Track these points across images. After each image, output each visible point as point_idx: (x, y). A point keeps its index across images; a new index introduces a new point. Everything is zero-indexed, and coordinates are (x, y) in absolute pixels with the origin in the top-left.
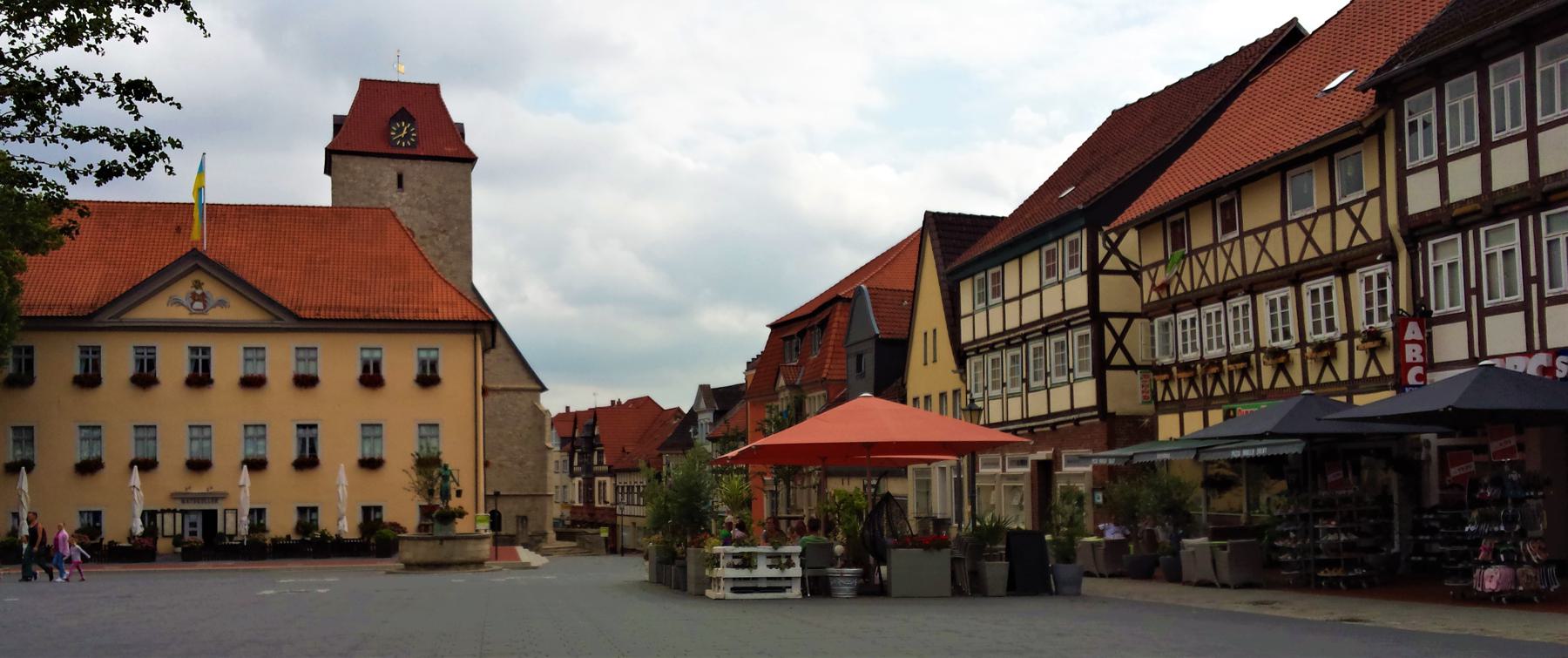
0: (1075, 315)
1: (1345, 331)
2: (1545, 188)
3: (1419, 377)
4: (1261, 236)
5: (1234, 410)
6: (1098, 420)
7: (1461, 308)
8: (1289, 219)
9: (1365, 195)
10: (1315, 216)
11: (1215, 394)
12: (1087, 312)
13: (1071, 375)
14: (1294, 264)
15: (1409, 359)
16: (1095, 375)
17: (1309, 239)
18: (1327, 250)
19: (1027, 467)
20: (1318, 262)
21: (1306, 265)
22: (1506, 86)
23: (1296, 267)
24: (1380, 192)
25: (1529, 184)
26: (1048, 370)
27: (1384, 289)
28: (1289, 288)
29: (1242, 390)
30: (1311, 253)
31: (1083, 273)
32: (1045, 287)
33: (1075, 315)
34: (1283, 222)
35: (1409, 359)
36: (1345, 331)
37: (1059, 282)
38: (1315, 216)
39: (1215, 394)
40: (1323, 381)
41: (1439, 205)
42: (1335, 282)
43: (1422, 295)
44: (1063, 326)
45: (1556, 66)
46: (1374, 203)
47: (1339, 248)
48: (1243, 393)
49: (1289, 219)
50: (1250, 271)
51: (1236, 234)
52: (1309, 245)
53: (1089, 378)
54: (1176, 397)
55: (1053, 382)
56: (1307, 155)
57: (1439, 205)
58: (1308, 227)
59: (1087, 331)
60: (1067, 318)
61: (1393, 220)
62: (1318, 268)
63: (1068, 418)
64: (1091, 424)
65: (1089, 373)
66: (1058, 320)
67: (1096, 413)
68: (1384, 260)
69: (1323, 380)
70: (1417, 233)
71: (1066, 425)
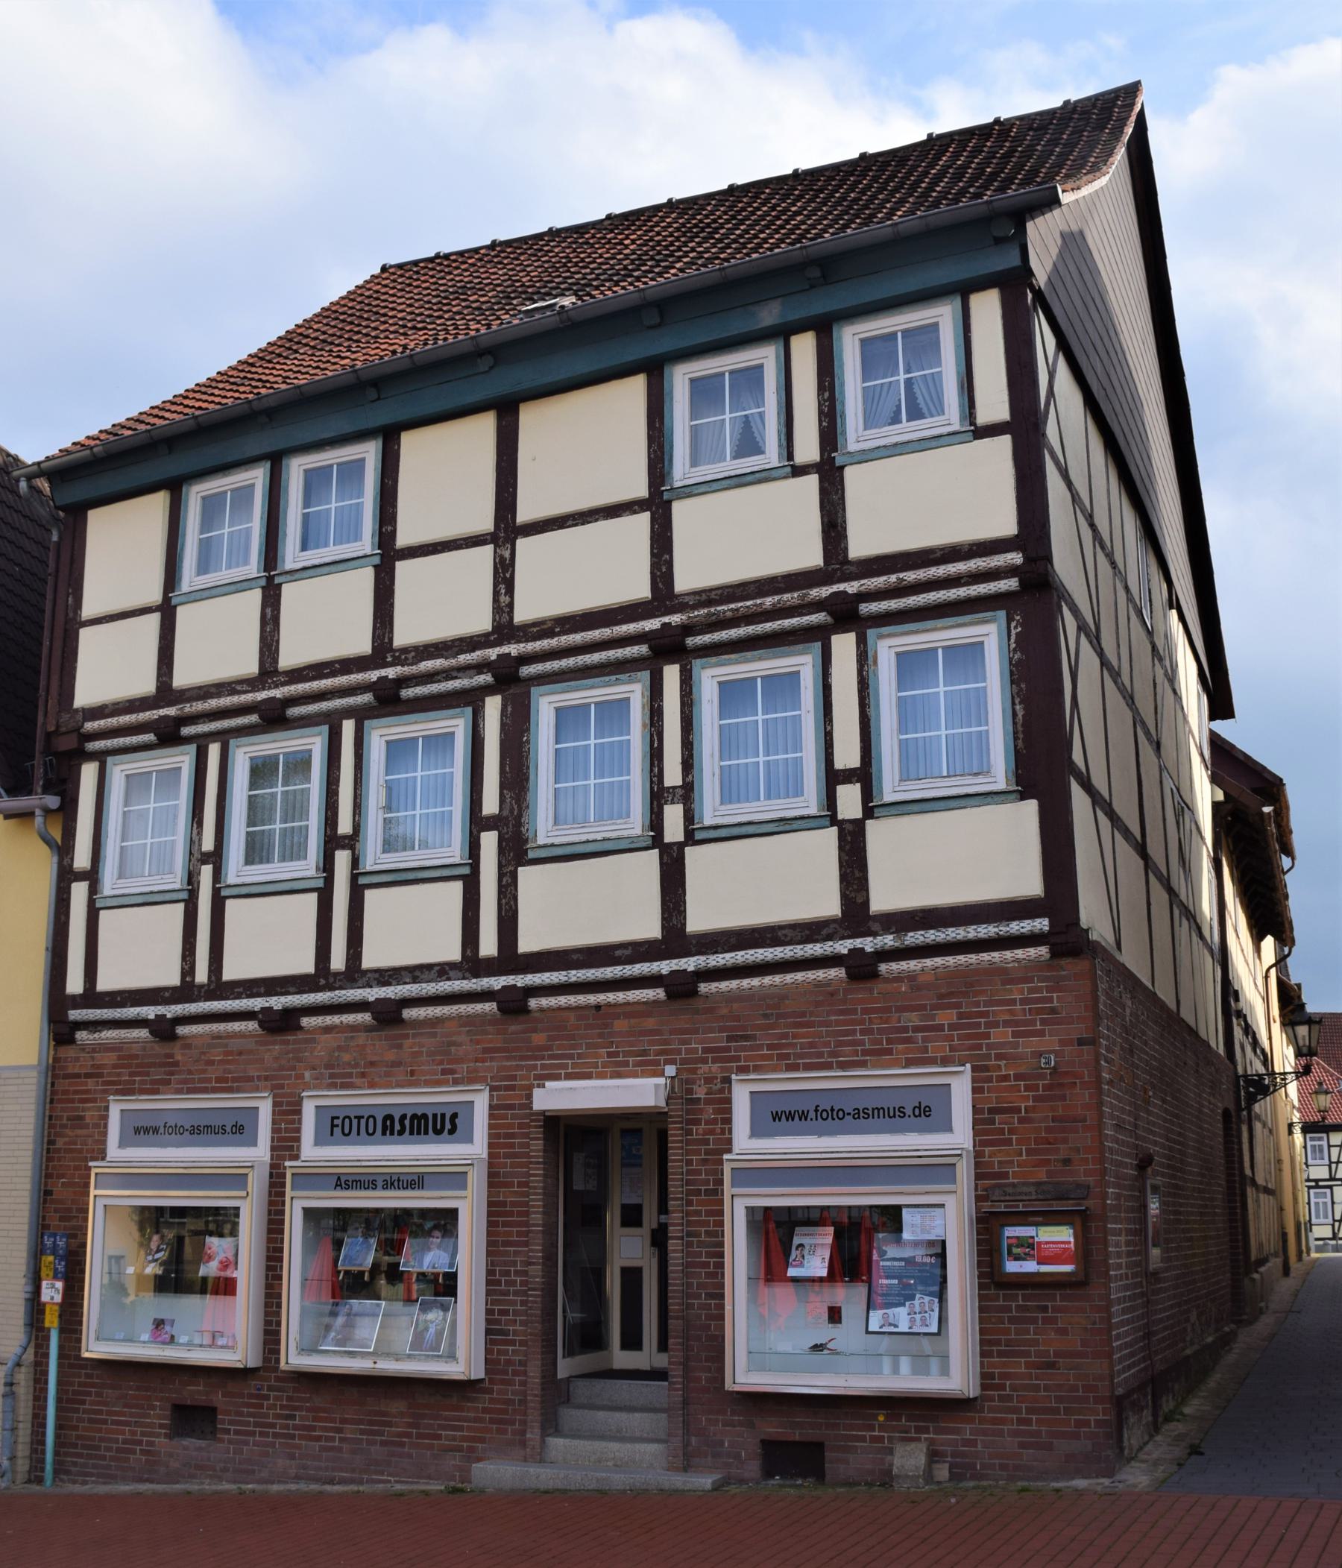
0: (910, 576)
6: (1042, 951)
32: (689, 491)
33: (910, 576)
64: (967, 979)
66: (790, 598)
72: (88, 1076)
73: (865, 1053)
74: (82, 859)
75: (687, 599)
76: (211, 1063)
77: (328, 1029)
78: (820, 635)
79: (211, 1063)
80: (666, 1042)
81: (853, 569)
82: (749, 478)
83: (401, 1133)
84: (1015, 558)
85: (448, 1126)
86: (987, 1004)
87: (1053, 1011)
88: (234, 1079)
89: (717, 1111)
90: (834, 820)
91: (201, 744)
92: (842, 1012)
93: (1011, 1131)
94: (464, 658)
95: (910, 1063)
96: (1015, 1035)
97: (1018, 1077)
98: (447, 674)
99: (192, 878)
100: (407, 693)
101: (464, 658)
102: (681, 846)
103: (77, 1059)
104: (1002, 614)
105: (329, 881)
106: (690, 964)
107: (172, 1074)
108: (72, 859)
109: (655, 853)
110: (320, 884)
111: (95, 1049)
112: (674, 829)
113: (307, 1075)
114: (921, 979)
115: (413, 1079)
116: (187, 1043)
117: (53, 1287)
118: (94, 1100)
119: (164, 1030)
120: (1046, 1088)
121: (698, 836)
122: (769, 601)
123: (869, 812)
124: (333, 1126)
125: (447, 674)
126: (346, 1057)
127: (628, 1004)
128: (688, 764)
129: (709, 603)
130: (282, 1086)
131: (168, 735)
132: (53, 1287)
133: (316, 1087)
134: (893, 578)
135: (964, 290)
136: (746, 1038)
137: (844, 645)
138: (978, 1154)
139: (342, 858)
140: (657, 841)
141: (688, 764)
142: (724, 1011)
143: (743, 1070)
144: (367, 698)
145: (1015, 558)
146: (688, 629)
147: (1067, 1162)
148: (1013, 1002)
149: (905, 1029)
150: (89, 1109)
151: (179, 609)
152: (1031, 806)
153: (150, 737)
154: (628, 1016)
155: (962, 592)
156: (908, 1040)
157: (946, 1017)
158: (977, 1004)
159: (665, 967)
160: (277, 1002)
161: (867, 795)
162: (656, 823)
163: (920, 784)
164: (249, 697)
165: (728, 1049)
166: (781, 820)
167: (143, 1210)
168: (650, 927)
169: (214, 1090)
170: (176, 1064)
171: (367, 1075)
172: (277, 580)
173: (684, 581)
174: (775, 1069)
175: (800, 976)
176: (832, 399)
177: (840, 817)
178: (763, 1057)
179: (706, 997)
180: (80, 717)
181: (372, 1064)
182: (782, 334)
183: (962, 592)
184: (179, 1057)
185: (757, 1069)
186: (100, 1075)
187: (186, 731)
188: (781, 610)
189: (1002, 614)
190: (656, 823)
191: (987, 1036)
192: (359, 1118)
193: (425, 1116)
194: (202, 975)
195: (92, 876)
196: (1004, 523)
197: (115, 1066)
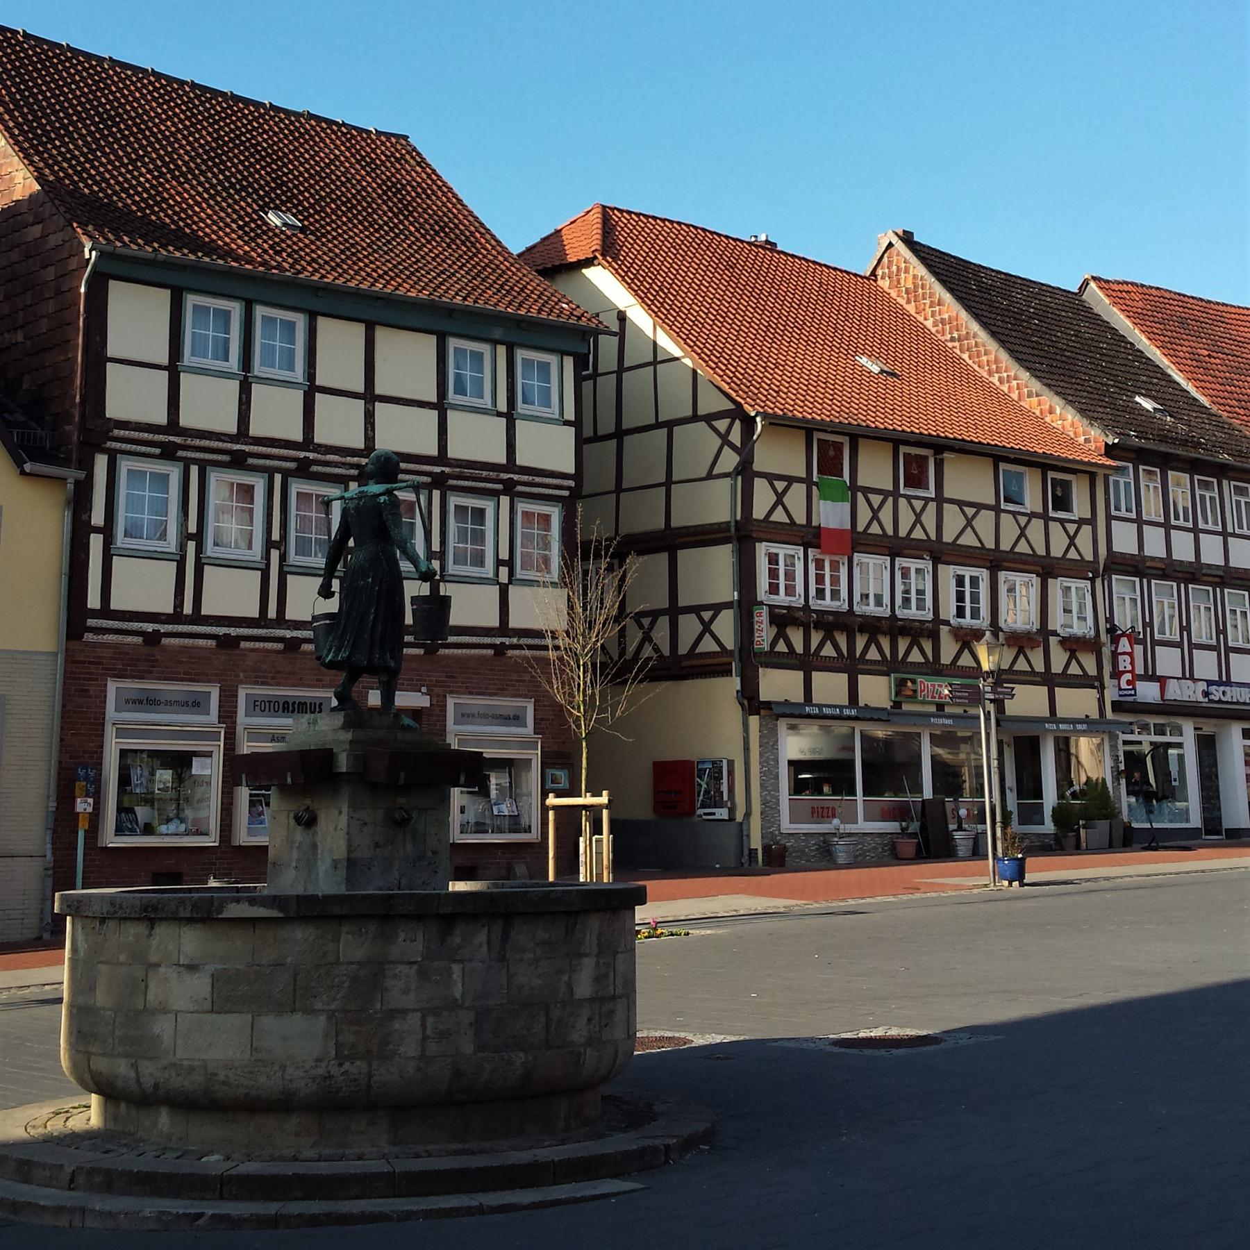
0: (538, 479)
3: (1128, 682)
14: (1003, 551)
15: (1121, 668)
20: (1030, 559)
24: (1092, 521)
33: (538, 479)
35: (1121, 668)
40: (1016, 668)
54: (799, 649)
62: (1026, 563)
63: (487, 640)
66: (493, 475)
69: (1016, 668)
72: (90, 663)
74: (98, 518)
76: (181, 662)
77: (253, 650)
79: (181, 662)
80: (421, 675)
83: (293, 711)
84: (572, 483)
85: (318, 709)
88: (196, 674)
89: (441, 711)
90: (498, 583)
91: (187, 463)
94: (349, 459)
98: (336, 465)
99: (182, 548)
100: (315, 468)
101: (349, 459)
102: (439, 581)
103: (83, 651)
105: (268, 565)
107: (153, 667)
108: (90, 517)
110: (178, 558)
111: (95, 645)
113: (241, 675)
115: (300, 684)
116: (165, 649)
117: (86, 802)
118: (97, 680)
119: (152, 639)
121: (447, 578)
122: (485, 473)
123: (510, 582)
124: (255, 706)
125: (336, 465)
126: (264, 667)
128: (443, 542)
130: (226, 680)
131: (168, 453)
132: (86, 802)
133: (246, 683)
134: (531, 478)
136: (453, 677)
139: (275, 554)
141: (443, 542)
143: (451, 692)
144: (292, 465)
145: (572, 483)
146: (450, 476)
147: (564, 743)
150: (92, 685)
153: (158, 451)
155: (550, 491)
156: (513, 685)
160: (233, 631)
161: (511, 573)
164: (229, 446)
165: (445, 682)
169: (182, 680)
170: (156, 661)
171: (275, 678)
172: (250, 380)
174: (464, 693)
175: (477, 651)
178: (459, 687)
180: (112, 425)
181: (279, 672)
183: (550, 491)
184: (158, 657)
185: (457, 692)
186: (102, 664)
187: (180, 453)
192: (270, 702)
193: (305, 703)
194: (188, 609)
195: (108, 530)
197: (112, 658)
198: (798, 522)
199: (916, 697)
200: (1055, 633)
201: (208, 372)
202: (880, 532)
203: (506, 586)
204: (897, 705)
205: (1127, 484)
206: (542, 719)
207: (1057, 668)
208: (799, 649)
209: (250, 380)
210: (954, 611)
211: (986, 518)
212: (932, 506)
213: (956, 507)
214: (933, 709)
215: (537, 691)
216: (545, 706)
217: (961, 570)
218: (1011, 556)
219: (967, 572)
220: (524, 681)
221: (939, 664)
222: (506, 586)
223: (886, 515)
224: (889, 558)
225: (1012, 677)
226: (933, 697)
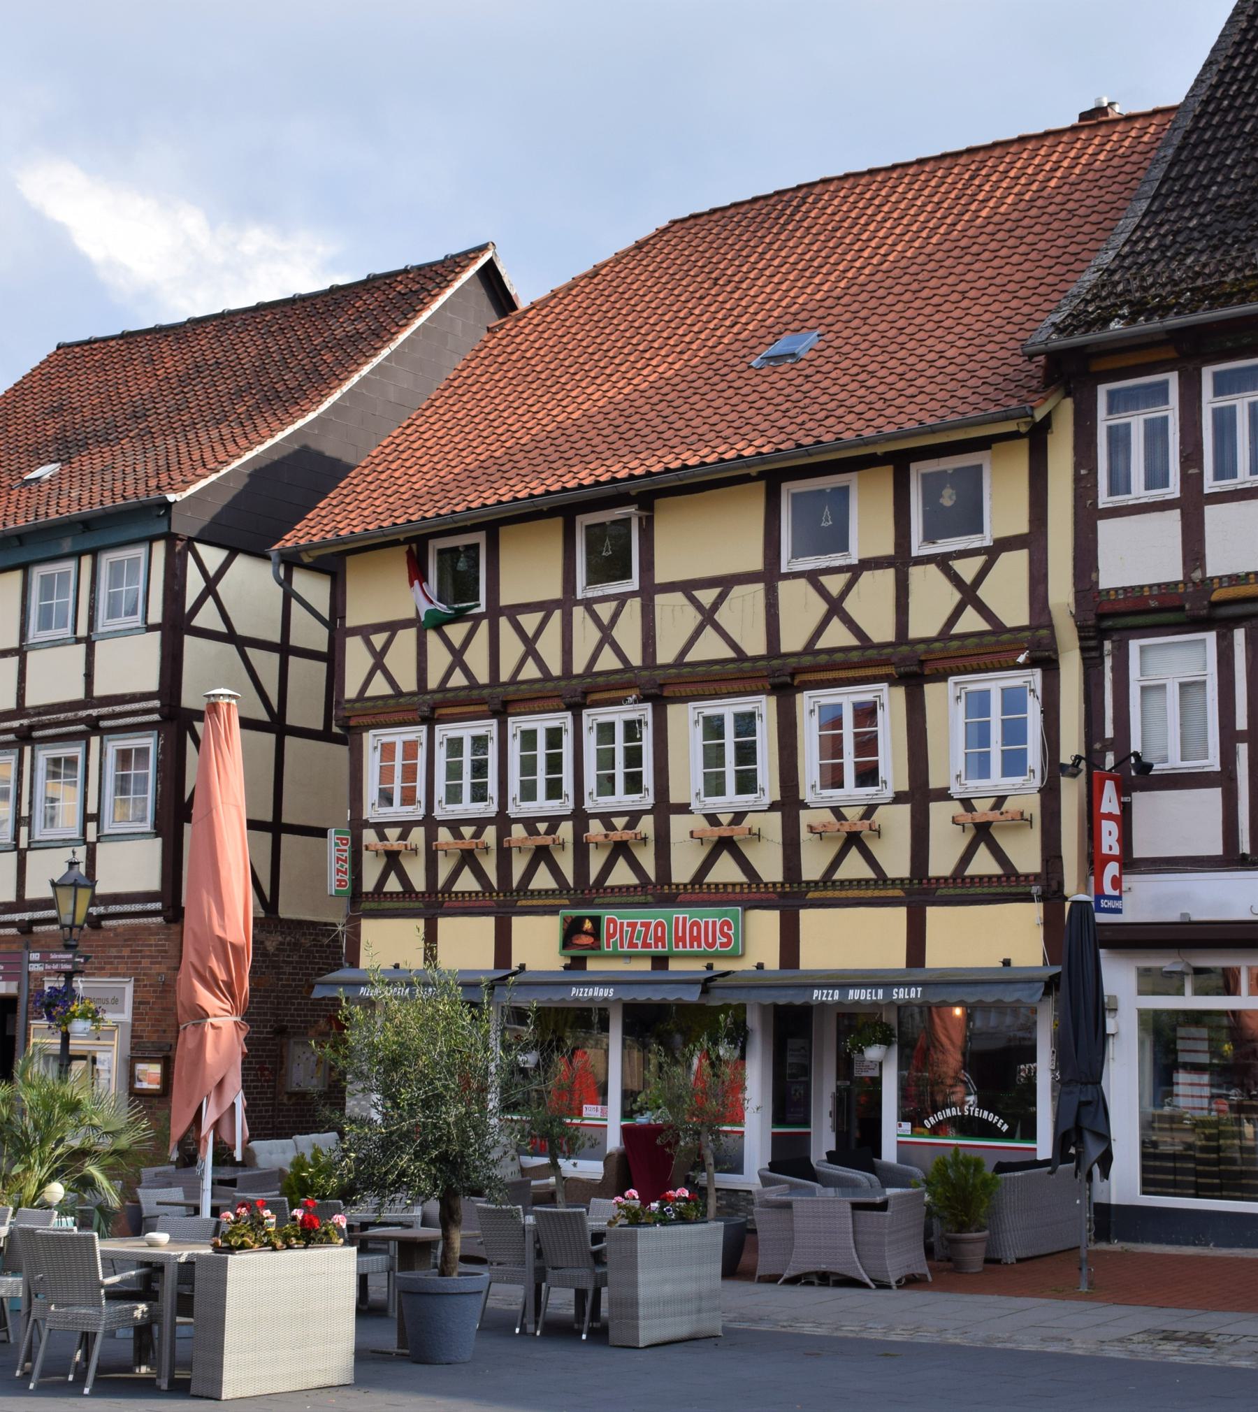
0: (118, 709)
1: (904, 786)
2: (1215, 597)
4: (378, 640)
5: (596, 921)
6: (160, 919)
7: (1213, 763)
8: (784, 569)
9: (988, 542)
10: (856, 571)
11: (386, 889)
12: (156, 703)
13: (24, 831)
16: (158, 830)
17: (379, 664)
18: (408, 683)
19: (123, 1012)
20: (855, 656)
21: (823, 658)
22: (1137, 423)
23: (793, 660)
25: (1181, 586)
26: (25, 812)
27: (612, 746)
28: (763, 697)
29: (612, 881)
30: (531, 671)
31: (150, 628)
32: (35, 647)
33: (118, 709)
34: (567, 602)
36: (904, 786)
37: (78, 641)
38: (856, 571)
39: (386, 889)
41: (1180, 578)
42: (765, 707)
43: (1109, 733)
44: (82, 727)
45: (1241, 403)
46: (1015, 564)
47: (915, 632)
48: (612, 888)
49: (784, 569)
50: (578, 667)
51: (634, 584)
52: (379, 675)
53: (143, 835)
54: (419, 884)
55: (37, 837)
56: (466, 526)
57: (1180, 578)
58: (605, 617)
59: (149, 742)
60: (94, 712)
61: (1061, 592)
64: (134, 929)
65: (147, 826)
66: (70, 715)
67: (158, 906)
68: (1031, 663)
70: (1108, 623)
71: (150, 920)
73: (96, 969)
75: (30, 711)
78: (84, 737)
81: (95, 702)
82: (59, 643)
86: (142, 946)
87: (165, 951)
90: (85, 842)
92: (88, 946)
93: (147, 1014)
95: (112, 975)
96: (152, 963)
97: (151, 986)
102: (26, 850)
104: (156, 732)
106: (27, 916)
109: (15, 853)
112: (92, 837)
114: (119, 930)
120: (161, 992)
121: (33, 846)
122: (62, 716)
123: (98, 838)
127: (5, 936)
129: (39, 714)
135: (151, 540)
137: (95, 741)
138: (133, 1025)
140: (16, 847)
142: (43, 942)
146: (32, 728)
147: (164, 1031)
148: (151, 945)
149: (110, 957)
151: (97, 643)
152: (159, 841)
154: (7, 942)
156: (111, 963)
157: (126, 952)
158: (138, 946)
159: (17, 917)
162: (16, 837)
163: (121, 825)
166: (64, 840)
167: (777, 1007)
168: (1214, 795)
172: (25, 649)
173: (30, 702)
176: (94, 599)
177: (88, 840)
179: (37, 933)
182: (78, 555)
188: (69, 721)
189: (156, 732)
190: (16, 837)
191: (140, 963)
196: (151, 682)
198: (405, 690)
199: (599, 948)
200: (943, 795)
201: (59, 643)
202: (852, 641)
203: (94, 844)
204: (578, 963)
205: (1156, 431)
206: (140, 1003)
207: (941, 864)
208: (419, 884)
209: (25, 649)
210: (699, 784)
211: (749, 599)
212: (634, 605)
213: (679, 597)
214: (646, 966)
215: (137, 968)
216: (145, 986)
217: (712, 708)
218: (807, 660)
219: (728, 709)
220: (123, 957)
221: (670, 884)
222: (94, 844)
223: (550, 647)
224: (569, 714)
225: (830, 894)
226: (632, 945)
